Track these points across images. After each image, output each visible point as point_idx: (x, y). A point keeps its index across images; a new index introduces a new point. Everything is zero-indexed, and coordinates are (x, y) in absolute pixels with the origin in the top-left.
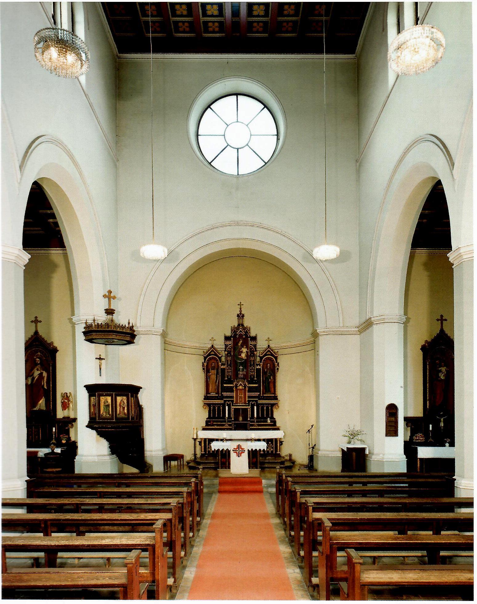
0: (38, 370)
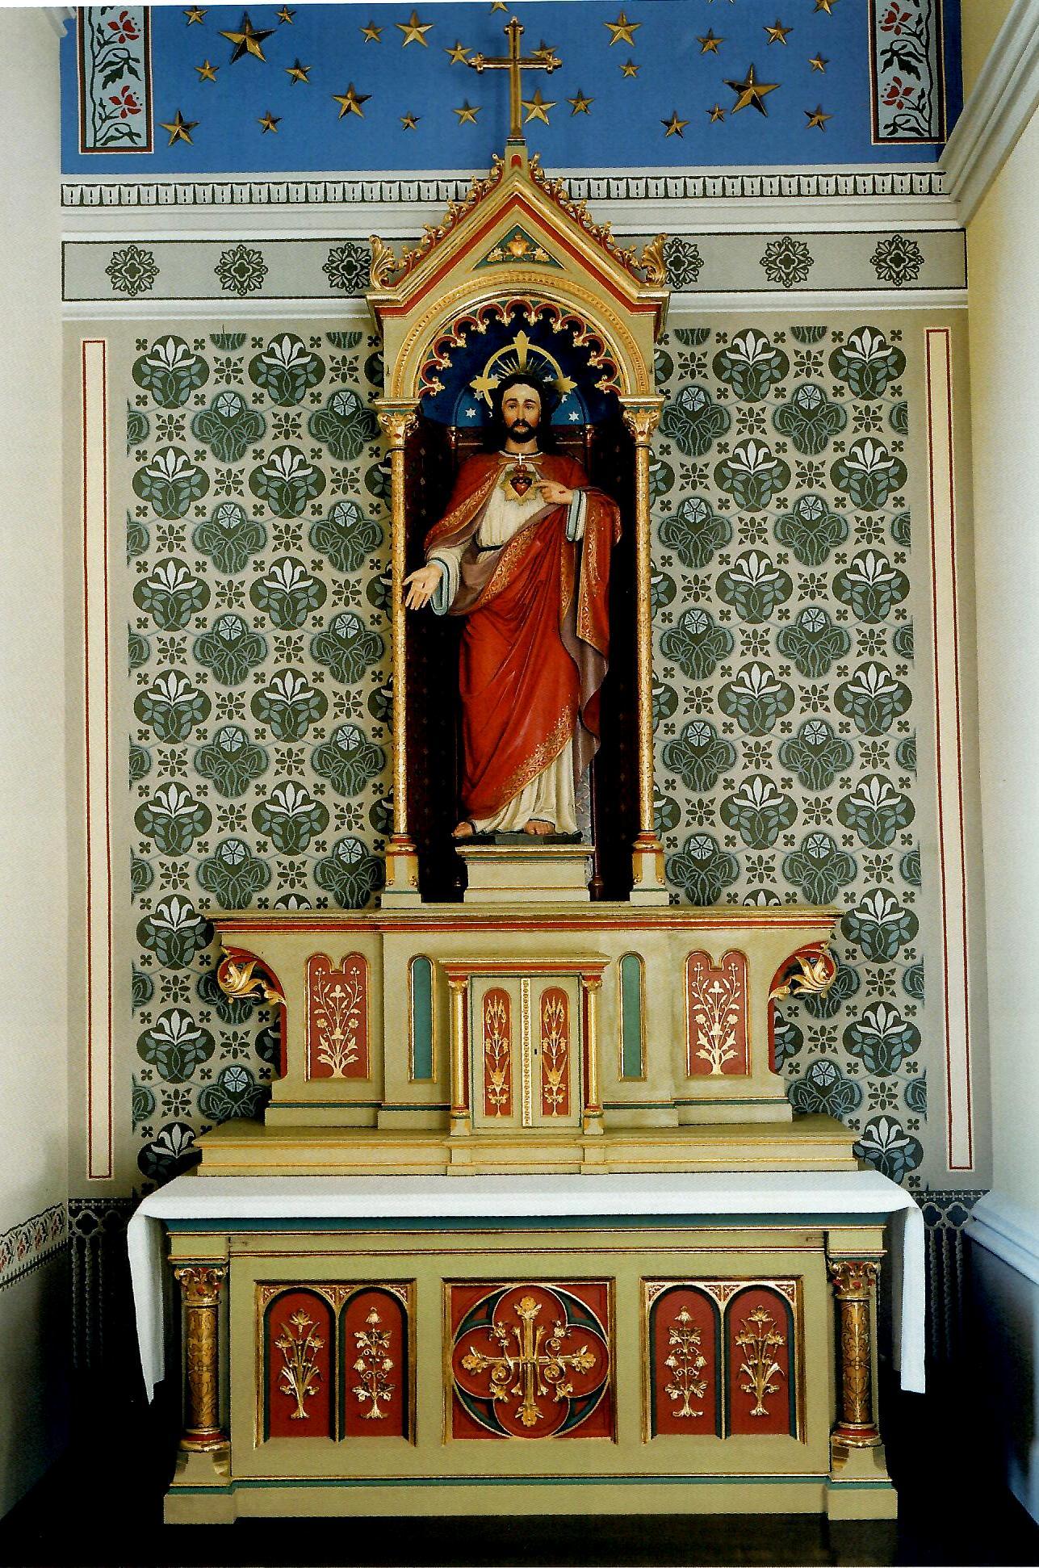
0: (521, 481)
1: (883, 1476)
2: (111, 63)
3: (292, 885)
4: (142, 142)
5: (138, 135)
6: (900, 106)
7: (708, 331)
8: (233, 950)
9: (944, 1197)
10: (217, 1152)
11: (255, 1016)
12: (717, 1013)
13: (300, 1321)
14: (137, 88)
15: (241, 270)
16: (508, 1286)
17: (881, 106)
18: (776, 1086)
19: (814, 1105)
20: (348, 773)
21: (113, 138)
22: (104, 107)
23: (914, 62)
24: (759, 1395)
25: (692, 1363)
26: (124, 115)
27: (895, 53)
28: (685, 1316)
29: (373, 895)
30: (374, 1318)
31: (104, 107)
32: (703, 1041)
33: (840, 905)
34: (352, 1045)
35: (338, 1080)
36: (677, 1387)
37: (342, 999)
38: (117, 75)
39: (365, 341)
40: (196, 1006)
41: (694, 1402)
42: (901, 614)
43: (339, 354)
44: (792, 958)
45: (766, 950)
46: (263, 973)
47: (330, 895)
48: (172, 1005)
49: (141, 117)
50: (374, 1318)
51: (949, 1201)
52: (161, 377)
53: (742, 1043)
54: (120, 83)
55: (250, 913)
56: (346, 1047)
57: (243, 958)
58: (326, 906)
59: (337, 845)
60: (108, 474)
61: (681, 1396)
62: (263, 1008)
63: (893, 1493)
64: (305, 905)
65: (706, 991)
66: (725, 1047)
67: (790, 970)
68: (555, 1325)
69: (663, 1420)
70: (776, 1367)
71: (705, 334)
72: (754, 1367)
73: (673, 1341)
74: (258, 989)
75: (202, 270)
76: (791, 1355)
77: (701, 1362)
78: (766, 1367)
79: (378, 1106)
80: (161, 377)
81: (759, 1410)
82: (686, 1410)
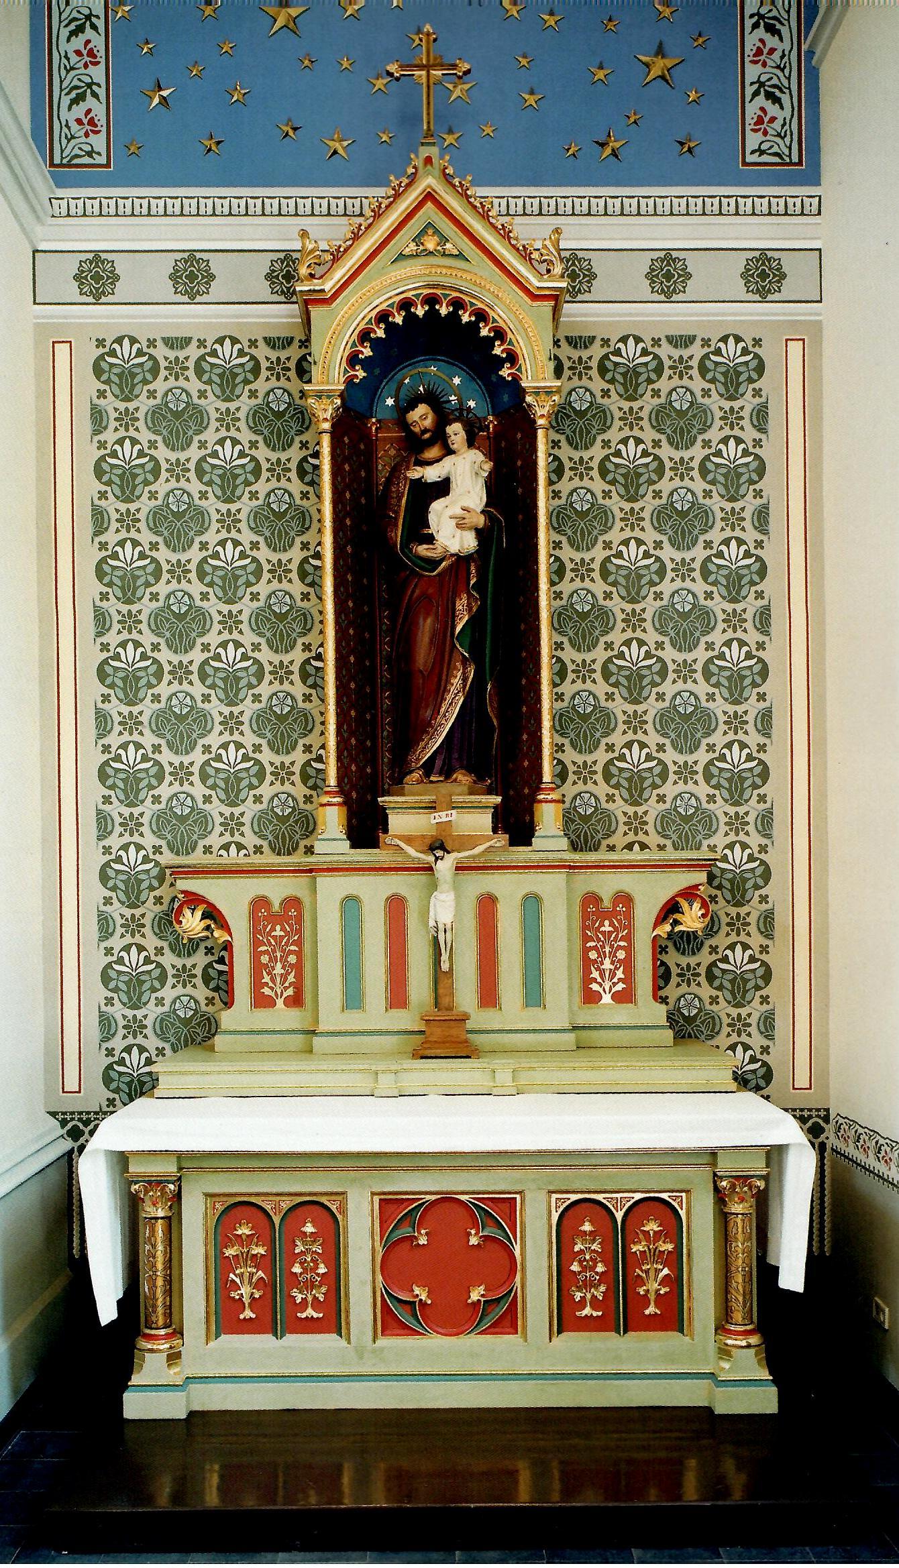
1: (765, 1375)
2: (75, 19)
4: (102, 160)
5: (99, 154)
6: (765, 133)
9: (806, 1114)
10: (174, 1071)
11: (202, 950)
12: (607, 949)
13: (244, 1230)
14: (99, 111)
15: (192, 276)
16: (428, 1197)
17: (748, 133)
18: (659, 1013)
19: (687, 1029)
20: (282, 733)
21: (77, 156)
22: (68, 59)
23: (778, 93)
24: (652, 1296)
25: (593, 1268)
26: (87, 135)
27: (762, 84)
28: (587, 1227)
31: (68, 59)
33: (704, 853)
34: (291, 978)
36: (579, 1289)
38: (80, 29)
39: (296, 343)
40: (151, 942)
41: (595, 1303)
43: (273, 355)
44: (673, 898)
45: (650, 893)
46: (213, 914)
48: (226, 535)
51: (810, 1117)
52: (120, 371)
53: (629, 979)
54: (82, 38)
55: (197, 858)
57: (193, 900)
60: (76, 454)
61: (583, 1298)
62: (209, 944)
63: (773, 1390)
64: (244, 851)
66: (615, 980)
67: (671, 909)
68: (470, 1234)
69: (565, 1319)
70: (666, 1271)
73: (577, 1249)
74: (208, 928)
75: (155, 278)
78: (657, 1271)
79: (313, 1032)
80: (120, 371)
81: (651, 1310)
82: (587, 1311)
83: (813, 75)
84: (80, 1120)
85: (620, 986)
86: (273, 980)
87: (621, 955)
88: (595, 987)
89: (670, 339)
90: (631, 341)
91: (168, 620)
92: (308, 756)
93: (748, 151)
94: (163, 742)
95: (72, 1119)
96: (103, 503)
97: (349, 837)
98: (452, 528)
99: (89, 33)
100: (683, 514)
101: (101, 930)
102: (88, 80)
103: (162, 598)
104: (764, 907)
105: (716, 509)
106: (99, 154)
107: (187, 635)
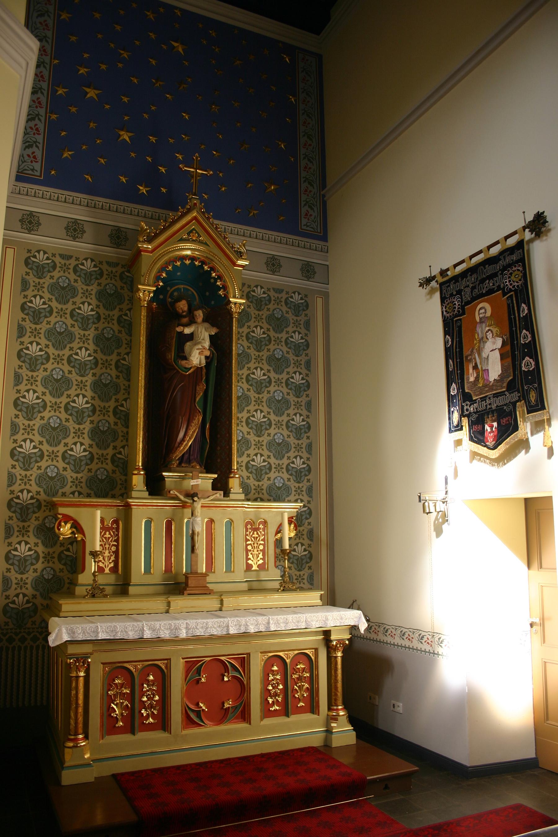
2: (29, 142)
3: (25, 484)
4: (38, 174)
5: (37, 171)
7: (283, 290)
8: (64, 516)
14: (38, 153)
22: (24, 158)
25: (152, 699)
27: (307, 202)
29: (272, 498)
30: (151, 678)
32: (250, 556)
35: (107, 574)
37: (109, 538)
42: (307, 396)
47: (41, 490)
49: (39, 164)
50: (151, 678)
56: (110, 558)
57: (67, 518)
58: (65, 496)
59: (97, 471)
65: (252, 536)
66: (259, 559)
68: (225, 675)
71: (282, 291)
72: (299, 687)
76: (313, 680)
77: (157, 698)
83: (325, 204)
84: (37, 632)
85: (261, 562)
86: (104, 559)
87: (261, 547)
88: (250, 562)
89: (274, 289)
90: (42, 253)
91: (51, 381)
92: (115, 451)
93: (302, 225)
94: (44, 440)
95: (33, 632)
96: (23, 323)
97: (148, 490)
98: (197, 357)
99: (37, 121)
100: (279, 360)
101: (6, 533)
102: (35, 140)
103: (49, 371)
104: (310, 527)
105: (291, 359)
106: (37, 171)
107: (60, 390)
